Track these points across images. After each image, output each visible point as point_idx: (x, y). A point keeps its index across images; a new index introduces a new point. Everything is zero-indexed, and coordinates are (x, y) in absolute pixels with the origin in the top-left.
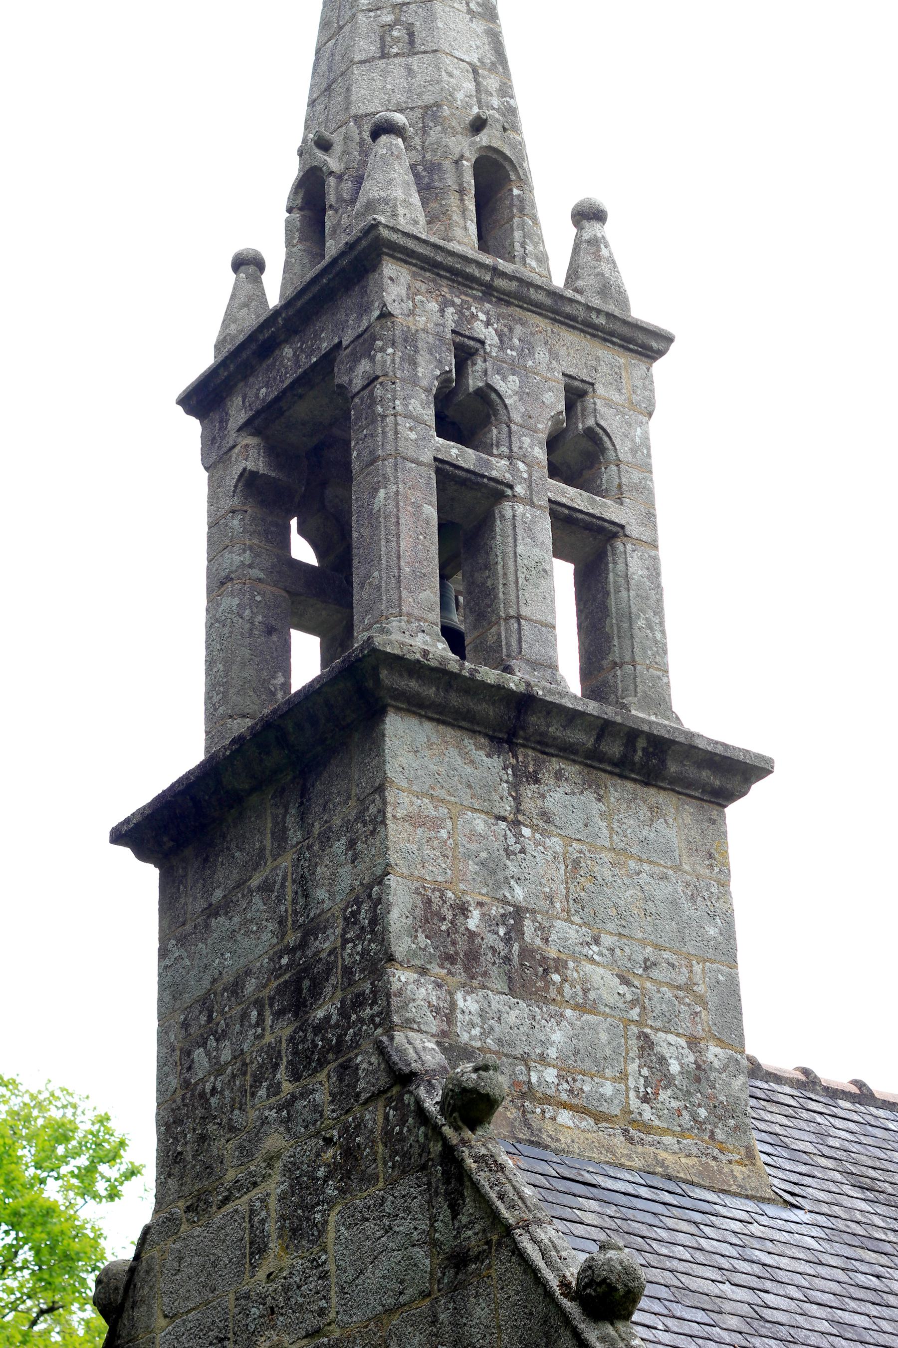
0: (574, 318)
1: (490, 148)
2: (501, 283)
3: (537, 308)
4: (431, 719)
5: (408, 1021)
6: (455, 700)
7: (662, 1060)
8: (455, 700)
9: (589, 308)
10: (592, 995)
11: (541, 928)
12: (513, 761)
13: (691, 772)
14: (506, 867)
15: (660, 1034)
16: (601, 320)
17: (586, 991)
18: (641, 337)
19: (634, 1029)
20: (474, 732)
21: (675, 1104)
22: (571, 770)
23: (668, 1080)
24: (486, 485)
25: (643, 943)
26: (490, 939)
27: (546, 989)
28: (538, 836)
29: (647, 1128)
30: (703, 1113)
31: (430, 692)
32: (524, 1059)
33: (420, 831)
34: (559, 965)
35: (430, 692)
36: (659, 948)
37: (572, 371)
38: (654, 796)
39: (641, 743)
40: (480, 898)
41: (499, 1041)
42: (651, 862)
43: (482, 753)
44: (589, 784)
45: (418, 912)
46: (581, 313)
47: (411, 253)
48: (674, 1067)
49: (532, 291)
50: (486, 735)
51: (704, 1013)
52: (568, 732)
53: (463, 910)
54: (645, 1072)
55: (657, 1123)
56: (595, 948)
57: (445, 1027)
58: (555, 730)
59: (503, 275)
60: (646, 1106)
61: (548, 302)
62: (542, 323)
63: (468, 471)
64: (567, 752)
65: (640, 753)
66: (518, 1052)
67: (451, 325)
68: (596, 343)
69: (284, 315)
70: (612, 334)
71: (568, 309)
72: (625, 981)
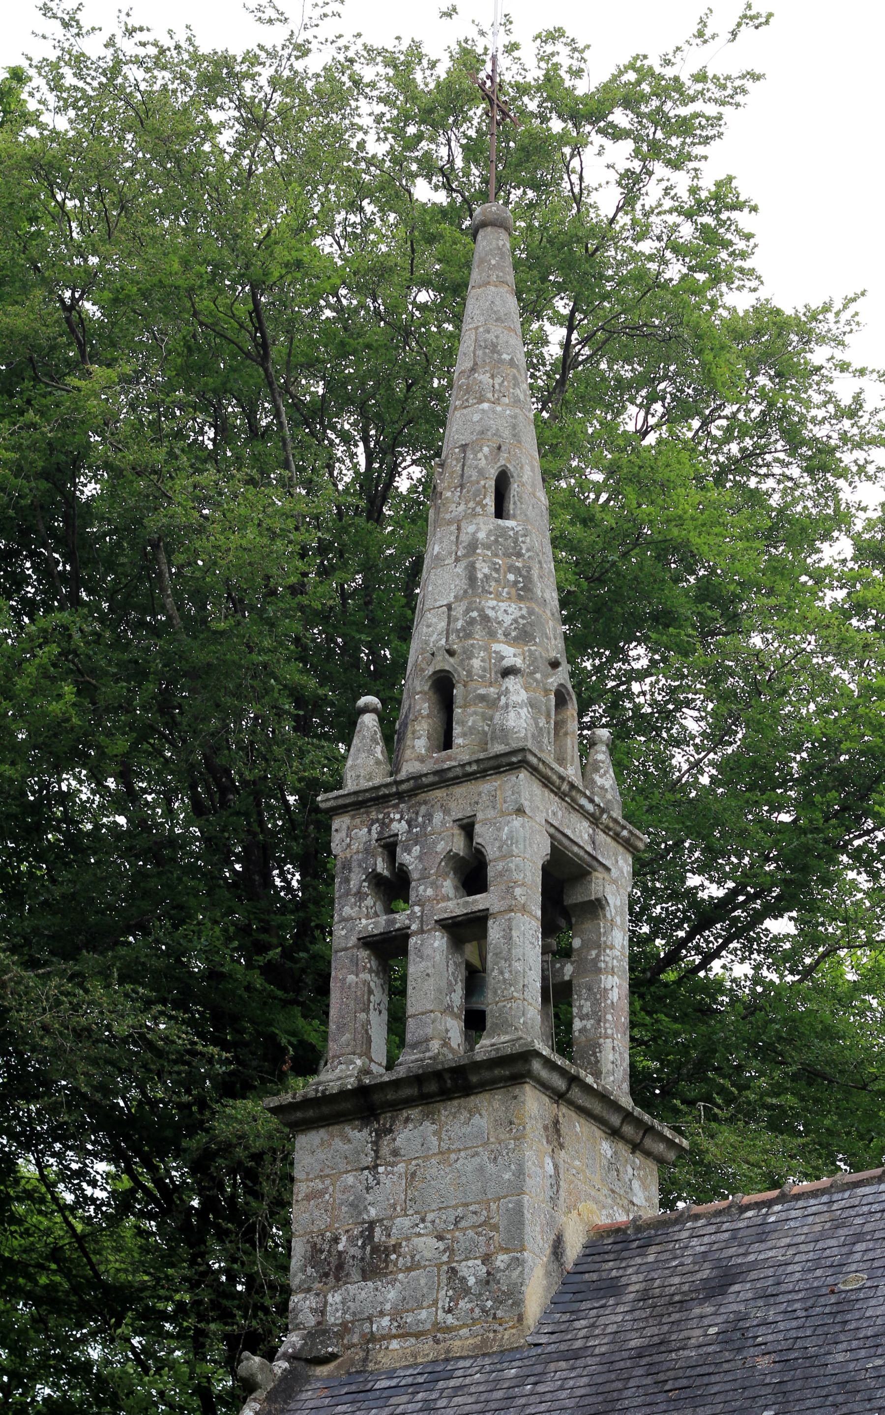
0: (457, 777)
1: (435, 673)
2: (404, 787)
3: (433, 786)
4: (323, 1126)
5: (298, 1325)
6: (326, 1110)
7: (463, 1279)
8: (326, 1110)
9: (463, 766)
10: (417, 1258)
11: (386, 1228)
12: (376, 1126)
13: (486, 1075)
14: (365, 1199)
15: (464, 1263)
16: (474, 767)
17: (413, 1257)
18: (504, 760)
19: (445, 1268)
20: (350, 1120)
21: (469, 1306)
22: (414, 1113)
23: (467, 1291)
24: (395, 936)
25: (455, 1207)
26: (353, 1251)
27: (387, 1267)
28: (389, 1168)
29: (448, 1329)
30: (489, 1304)
31: (310, 1113)
32: (370, 1319)
33: (312, 1202)
34: (396, 1247)
35: (310, 1113)
36: (466, 1205)
37: (460, 816)
38: (474, 1101)
39: (447, 1076)
40: (347, 1228)
41: (354, 1314)
42: (466, 1149)
43: (356, 1131)
44: (428, 1115)
45: (309, 1254)
46: (459, 771)
47: (345, 806)
48: (472, 1281)
49: (424, 779)
50: (358, 1119)
51: (497, 1235)
52: (400, 1093)
53: (336, 1240)
54: (450, 1293)
55: (456, 1323)
56: (422, 1226)
57: (320, 1319)
58: (390, 1096)
59: (402, 782)
60: (450, 1315)
61: (436, 779)
62: (439, 793)
63: (381, 934)
64: (408, 1103)
65: (449, 1081)
66: (365, 1316)
67: (375, 836)
68: (480, 782)
69: (118, 964)
70: (485, 770)
71: (451, 775)
72: (440, 1238)
